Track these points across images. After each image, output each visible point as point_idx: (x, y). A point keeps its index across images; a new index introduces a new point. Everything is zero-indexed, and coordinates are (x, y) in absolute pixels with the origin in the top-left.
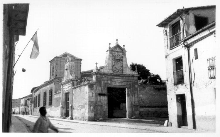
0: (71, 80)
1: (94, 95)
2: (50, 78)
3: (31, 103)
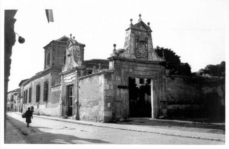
0: (77, 68)
1: (112, 87)
2: (45, 68)
3: (19, 99)
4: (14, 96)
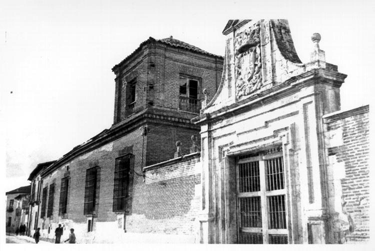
2: (117, 119)
4: (15, 200)
